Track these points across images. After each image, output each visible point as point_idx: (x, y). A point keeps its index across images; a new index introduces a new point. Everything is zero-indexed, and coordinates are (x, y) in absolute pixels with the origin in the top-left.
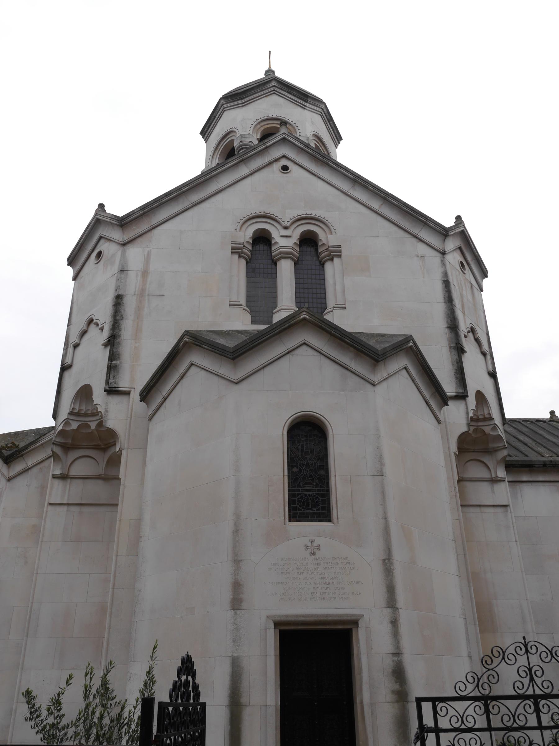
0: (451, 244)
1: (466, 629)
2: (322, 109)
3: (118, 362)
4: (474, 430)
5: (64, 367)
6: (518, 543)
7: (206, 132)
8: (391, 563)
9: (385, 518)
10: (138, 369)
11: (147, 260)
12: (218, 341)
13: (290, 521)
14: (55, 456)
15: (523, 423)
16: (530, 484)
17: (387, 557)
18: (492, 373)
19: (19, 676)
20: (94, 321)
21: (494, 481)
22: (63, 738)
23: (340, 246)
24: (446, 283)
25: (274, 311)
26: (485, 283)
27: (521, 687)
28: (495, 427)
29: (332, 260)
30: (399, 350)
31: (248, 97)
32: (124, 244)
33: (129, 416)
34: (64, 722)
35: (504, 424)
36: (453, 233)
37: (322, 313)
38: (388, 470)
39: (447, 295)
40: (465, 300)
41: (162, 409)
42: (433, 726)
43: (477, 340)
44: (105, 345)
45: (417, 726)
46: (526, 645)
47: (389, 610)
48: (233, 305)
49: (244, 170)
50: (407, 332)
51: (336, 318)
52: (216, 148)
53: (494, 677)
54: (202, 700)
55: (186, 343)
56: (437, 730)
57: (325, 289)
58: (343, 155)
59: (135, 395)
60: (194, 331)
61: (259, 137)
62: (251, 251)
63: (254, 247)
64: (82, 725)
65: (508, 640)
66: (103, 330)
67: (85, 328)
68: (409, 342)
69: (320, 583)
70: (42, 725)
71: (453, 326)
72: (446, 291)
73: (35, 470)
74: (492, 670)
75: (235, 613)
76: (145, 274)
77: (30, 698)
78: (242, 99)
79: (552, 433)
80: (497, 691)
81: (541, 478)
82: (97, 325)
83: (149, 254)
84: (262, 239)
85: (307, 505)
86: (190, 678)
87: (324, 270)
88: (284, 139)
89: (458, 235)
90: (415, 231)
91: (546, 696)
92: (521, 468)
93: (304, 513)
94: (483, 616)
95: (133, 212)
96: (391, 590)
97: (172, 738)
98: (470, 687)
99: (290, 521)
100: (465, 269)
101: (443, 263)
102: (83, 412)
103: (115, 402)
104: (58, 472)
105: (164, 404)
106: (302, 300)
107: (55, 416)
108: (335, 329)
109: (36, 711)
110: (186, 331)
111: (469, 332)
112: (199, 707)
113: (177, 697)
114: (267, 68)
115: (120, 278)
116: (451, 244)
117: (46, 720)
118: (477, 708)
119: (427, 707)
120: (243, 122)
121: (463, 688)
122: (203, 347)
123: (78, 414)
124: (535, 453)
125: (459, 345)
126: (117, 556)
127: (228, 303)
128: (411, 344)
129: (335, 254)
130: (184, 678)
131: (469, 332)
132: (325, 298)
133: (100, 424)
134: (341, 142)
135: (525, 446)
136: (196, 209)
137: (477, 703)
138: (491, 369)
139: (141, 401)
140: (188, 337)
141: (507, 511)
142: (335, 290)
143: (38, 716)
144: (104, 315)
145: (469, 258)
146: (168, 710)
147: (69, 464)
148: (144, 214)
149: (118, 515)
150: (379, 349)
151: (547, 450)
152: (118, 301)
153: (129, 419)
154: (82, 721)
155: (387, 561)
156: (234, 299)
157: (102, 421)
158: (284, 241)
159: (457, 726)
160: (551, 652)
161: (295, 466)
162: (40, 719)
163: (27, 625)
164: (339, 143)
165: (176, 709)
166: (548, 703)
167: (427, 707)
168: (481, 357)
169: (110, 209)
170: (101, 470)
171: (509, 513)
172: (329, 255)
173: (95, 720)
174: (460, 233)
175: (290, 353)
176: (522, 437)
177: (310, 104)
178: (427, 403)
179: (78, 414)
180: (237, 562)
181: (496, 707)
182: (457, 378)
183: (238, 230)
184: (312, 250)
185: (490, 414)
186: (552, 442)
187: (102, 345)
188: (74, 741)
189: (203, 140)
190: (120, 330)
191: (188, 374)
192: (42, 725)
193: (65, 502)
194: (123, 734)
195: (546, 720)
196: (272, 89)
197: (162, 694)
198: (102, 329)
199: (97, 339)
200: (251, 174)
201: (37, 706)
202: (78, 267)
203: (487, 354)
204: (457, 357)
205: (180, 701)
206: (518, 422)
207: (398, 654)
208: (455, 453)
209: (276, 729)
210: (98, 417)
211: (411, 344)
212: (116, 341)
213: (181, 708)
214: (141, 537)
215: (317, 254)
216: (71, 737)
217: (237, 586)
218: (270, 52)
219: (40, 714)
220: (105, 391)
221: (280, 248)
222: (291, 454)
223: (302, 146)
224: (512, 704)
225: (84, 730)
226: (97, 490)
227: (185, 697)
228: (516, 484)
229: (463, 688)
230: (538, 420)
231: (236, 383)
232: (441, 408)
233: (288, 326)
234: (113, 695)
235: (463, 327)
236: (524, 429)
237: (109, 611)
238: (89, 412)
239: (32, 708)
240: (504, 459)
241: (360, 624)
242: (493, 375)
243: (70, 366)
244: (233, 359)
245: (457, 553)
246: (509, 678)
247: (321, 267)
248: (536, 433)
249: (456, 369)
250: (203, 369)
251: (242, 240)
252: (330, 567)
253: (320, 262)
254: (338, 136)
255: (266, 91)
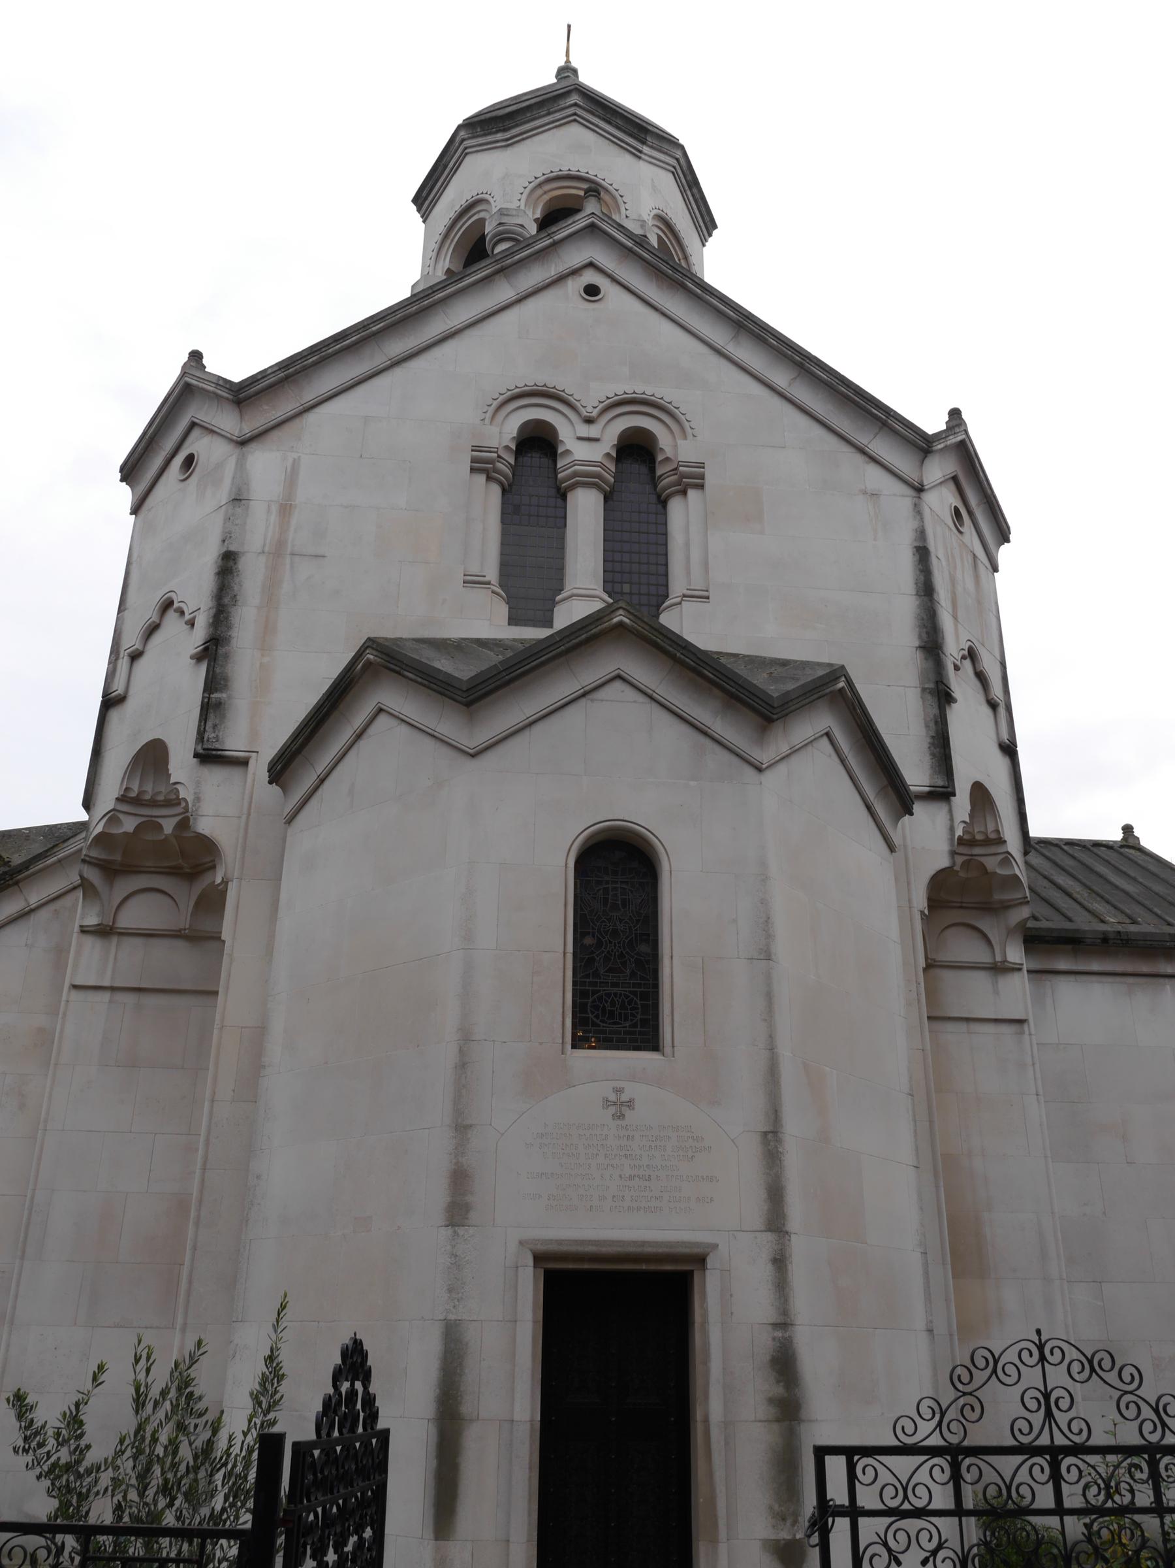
0: (937, 470)
1: (926, 1274)
2: (677, 160)
3: (224, 695)
4: (963, 864)
5: (109, 700)
6: (1042, 1099)
7: (426, 199)
8: (779, 1141)
9: (772, 1048)
10: (265, 719)
11: (291, 478)
12: (437, 665)
13: (574, 1047)
14: (85, 885)
15: (1065, 848)
16: (1072, 978)
17: (771, 1128)
18: (1008, 746)
19: (4, 1337)
20: (176, 605)
21: (1000, 969)
22: (89, 1491)
23: (701, 465)
24: (922, 554)
25: (558, 598)
26: (1004, 554)
27: (1026, 1431)
28: (1007, 859)
29: (684, 493)
30: (816, 696)
31: (517, 125)
32: (243, 443)
33: (245, 811)
34: (91, 1458)
35: (1026, 853)
36: (940, 447)
37: (659, 606)
38: (781, 948)
39: (922, 578)
40: (959, 589)
41: (314, 802)
42: (847, 1504)
43: (981, 676)
44: (198, 658)
45: (815, 1503)
46: (1041, 1347)
47: (769, 1236)
48: (471, 582)
49: (504, 291)
50: (836, 661)
51: (686, 621)
52: (446, 236)
53: (973, 1409)
54: (381, 1425)
55: (369, 663)
56: (854, 1512)
57: (666, 555)
58: (720, 265)
59: (259, 768)
60: (386, 639)
61: (538, 215)
62: (514, 469)
63: (520, 459)
64: (131, 1463)
65: (1007, 1335)
66: (193, 625)
67: (155, 618)
68: (837, 679)
69: (631, 1178)
70: (49, 1462)
71: (931, 645)
72: (921, 571)
73: (44, 914)
74: (970, 1394)
75: (455, 1232)
76: (286, 509)
77: (24, 1409)
78: (505, 130)
79: (1125, 873)
80: (978, 1437)
81: (1095, 966)
82: (182, 613)
83: (295, 465)
84: (537, 443)
85: (612, 1015)
86: (358, 1385)
87: (665, 514)
88: (592, 227)
89: (953, 452)
90: (862, 439)
91: (1076, 1450)
92: (1055, 945)
93: (604, 1032)
94: (963, 1248)
95: (263, 375)
96: (775, 1195)
97: (319, 1510)
98: (925, 1428)
99: (574, 1047)
100: (962, 524)
101: (918, 511)
102: (147, 797)
103: (215, 776)
104: (92, 920)
105: (320, 789)
106: (617, 557)
107: (87, 804)
108: (684, 648)
109: (37, 1433)
110: (369, 639)
111: (964, 657)
112: (374, 1441)
113: (332, 1427)
114: (562, 63)
115: (233, 515)
116: (937, 470)
117: (57, 1451)
118: (936, 1470)
119: (836, 1466)
120: (506, 182)
121: (910, 1429)
122: (404, 676)
123: (137, 801)
124: (1086, 913)
125: (941, 687)
126: (213, 1101)
127: (461, 578)
128: (841, 684)
129: (691, 480)
130: (345, 1386)
131: (964, 657)
132: (667, 575)
133: (184, 824)
134: (715, 232)
135: (1067, 898)
136: (398, 372)
137: (936, 1460)
138: (1005, 737)
139: (270, 782)
140: (375, 652)
141: (1022, 1033)
142: (688, 559)
143: (41, 1445)
144: (197, 594)
145: (973, 499)
146: (312, 1455)
147: (115, 904)
148: (287, 378)
149: (218, 1017)
150: (775, 695)
151: (1111, 908)
152: (228, 564)
153: (244, 817)
154: (128, 1453)
155: (770, 1136)
156: (474, 569)
157: (187, 819)
158: (585, 448)
159: (893, 1504)
160: (1090, 1362)
161: (588, 933)
162: (45, 1450)
163: (22, 1235)
164: (710, 235)
165: (328, 1452)
166: (1080, 1463)
167: (836, 1466)
168: (986, 710)
169: (213, 365)
170: (183, 920)
171: (1026, 1036)
172: (679, 483)
173: (160, 1450)
174: (956, 447)
175: (589, 697)
176: (1062, 880)
177: (651, 147)
178: (869, 808)
179: (137, 801)
180: (461, 1128)
181: (974, 1469)
182: (933, 755)
183: (487, 421)
184: (644, 470)
185: (998, 831)
186: (1123, 891)
187: (192, 658)
188: (113, 1496)
189: (417, 217)
190: (229, 627)
191: (372, 730)
192: (49, 1462)
193: (106, 983)
194: (219, 1483)
195: (1073, 1498)
196: (462, 147)
197: (298, 1422)
198: (189, 621)
199: (180, 643)
200: (519, 301)
201: (38, 1424)
202: (143, 486)
203: (999, 705)
204: (936, 711)
205: (336, 1434)
206: (1056, 845)
207: (783, 1324)
208: (922, 912)
209: (530, 1468)
210: (179, 810)
211: (842, 684)
212: (221, 651)
213: (338, 1449)
214: (264, 1067)
215: (654, 480)
216: (106, 1489)
217: (460, 1179)
218: (569, 26)
219: (45, 1441)
220: (196, 755)
221: (574, 463)
222: (582, 909)
223: (629, 244)
224: (1007, 1464)
225: (134, 1476)
226: (174, 962)
227: (348, 1425)
228: (1044, 977)
229: (910, 1429)
230: (1097, 844)
231: (473, 756)
232: (897, 818)
233: (585, 638)
234: (201, 1406)
235: (953, 648)
236: (1068, 863)
237: (193, 1214)
238: (161, 798)
239: (27, 1428)
240: (1022, 925)
241: (710, 1262)
242: (1009, 750)
243: (121, 699)
244: (468, 704)
245: (915, 1121)
246: (1003, 1413)
247: (660, 507)
248: (1091, 870)
249: (933, 737)
250: (403, 720)
251: (494, 443)
252: (653, 1144)
253: (659, 496)
254: (707, 219)
255: (558, 116)
